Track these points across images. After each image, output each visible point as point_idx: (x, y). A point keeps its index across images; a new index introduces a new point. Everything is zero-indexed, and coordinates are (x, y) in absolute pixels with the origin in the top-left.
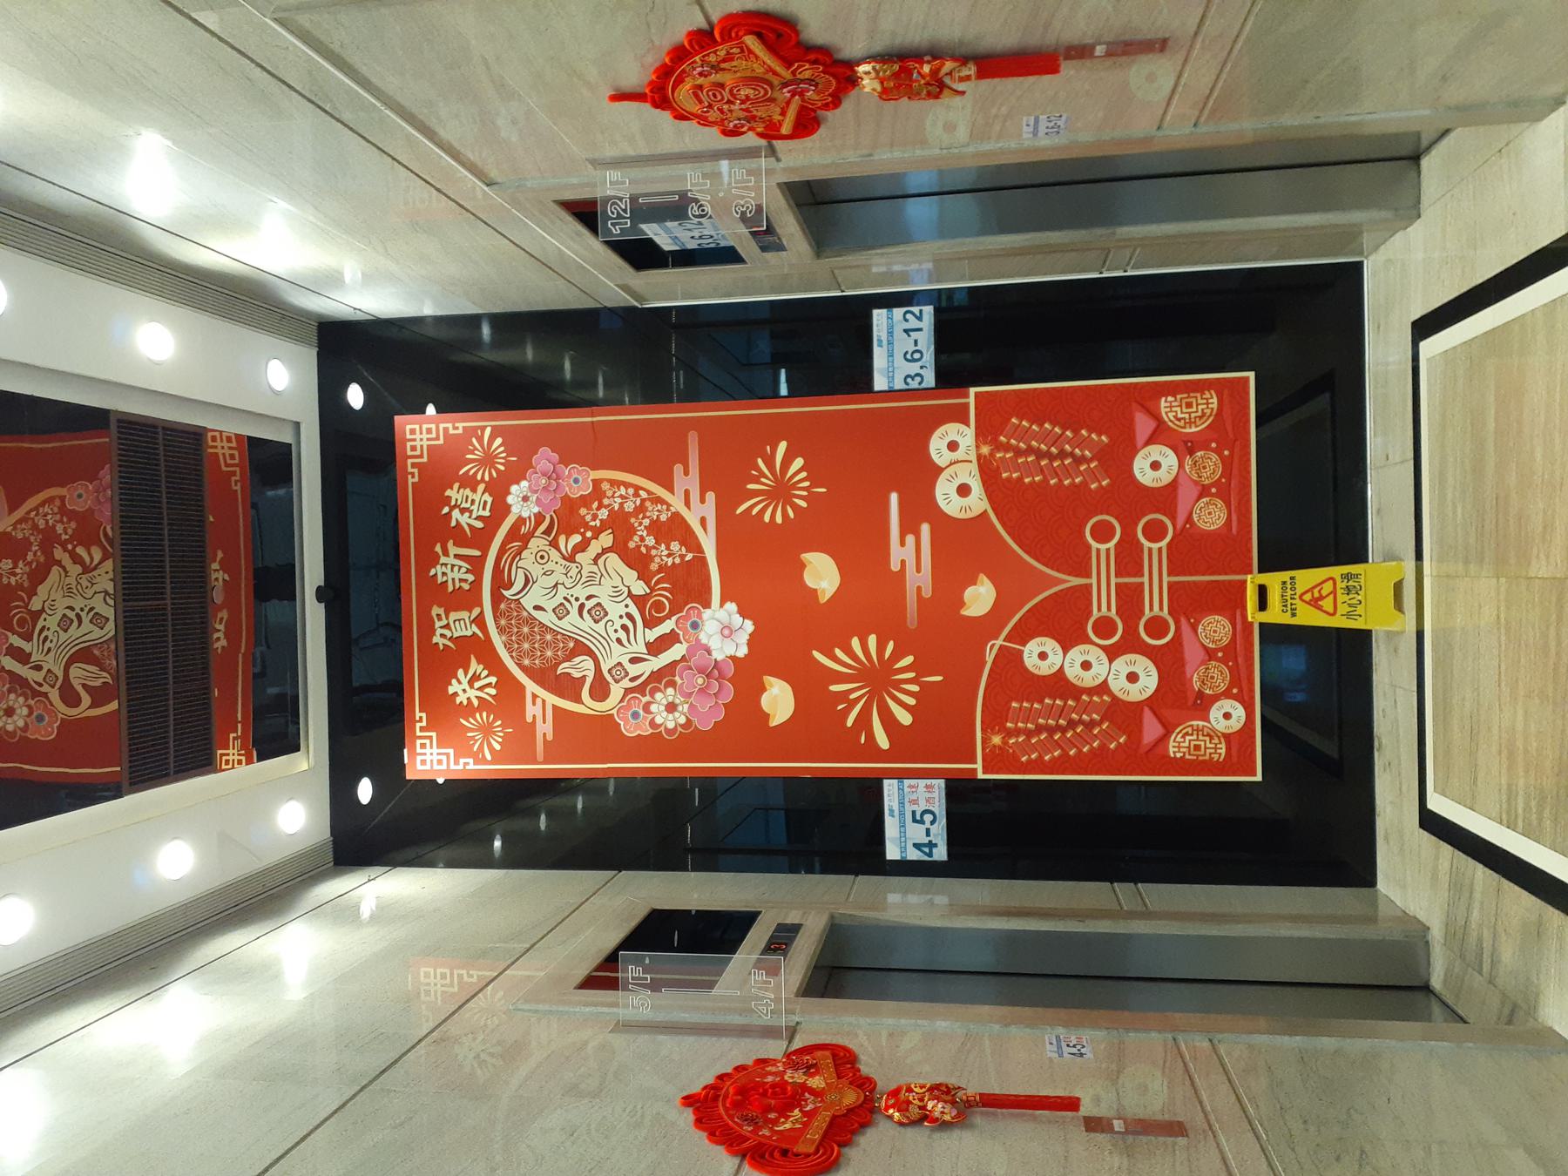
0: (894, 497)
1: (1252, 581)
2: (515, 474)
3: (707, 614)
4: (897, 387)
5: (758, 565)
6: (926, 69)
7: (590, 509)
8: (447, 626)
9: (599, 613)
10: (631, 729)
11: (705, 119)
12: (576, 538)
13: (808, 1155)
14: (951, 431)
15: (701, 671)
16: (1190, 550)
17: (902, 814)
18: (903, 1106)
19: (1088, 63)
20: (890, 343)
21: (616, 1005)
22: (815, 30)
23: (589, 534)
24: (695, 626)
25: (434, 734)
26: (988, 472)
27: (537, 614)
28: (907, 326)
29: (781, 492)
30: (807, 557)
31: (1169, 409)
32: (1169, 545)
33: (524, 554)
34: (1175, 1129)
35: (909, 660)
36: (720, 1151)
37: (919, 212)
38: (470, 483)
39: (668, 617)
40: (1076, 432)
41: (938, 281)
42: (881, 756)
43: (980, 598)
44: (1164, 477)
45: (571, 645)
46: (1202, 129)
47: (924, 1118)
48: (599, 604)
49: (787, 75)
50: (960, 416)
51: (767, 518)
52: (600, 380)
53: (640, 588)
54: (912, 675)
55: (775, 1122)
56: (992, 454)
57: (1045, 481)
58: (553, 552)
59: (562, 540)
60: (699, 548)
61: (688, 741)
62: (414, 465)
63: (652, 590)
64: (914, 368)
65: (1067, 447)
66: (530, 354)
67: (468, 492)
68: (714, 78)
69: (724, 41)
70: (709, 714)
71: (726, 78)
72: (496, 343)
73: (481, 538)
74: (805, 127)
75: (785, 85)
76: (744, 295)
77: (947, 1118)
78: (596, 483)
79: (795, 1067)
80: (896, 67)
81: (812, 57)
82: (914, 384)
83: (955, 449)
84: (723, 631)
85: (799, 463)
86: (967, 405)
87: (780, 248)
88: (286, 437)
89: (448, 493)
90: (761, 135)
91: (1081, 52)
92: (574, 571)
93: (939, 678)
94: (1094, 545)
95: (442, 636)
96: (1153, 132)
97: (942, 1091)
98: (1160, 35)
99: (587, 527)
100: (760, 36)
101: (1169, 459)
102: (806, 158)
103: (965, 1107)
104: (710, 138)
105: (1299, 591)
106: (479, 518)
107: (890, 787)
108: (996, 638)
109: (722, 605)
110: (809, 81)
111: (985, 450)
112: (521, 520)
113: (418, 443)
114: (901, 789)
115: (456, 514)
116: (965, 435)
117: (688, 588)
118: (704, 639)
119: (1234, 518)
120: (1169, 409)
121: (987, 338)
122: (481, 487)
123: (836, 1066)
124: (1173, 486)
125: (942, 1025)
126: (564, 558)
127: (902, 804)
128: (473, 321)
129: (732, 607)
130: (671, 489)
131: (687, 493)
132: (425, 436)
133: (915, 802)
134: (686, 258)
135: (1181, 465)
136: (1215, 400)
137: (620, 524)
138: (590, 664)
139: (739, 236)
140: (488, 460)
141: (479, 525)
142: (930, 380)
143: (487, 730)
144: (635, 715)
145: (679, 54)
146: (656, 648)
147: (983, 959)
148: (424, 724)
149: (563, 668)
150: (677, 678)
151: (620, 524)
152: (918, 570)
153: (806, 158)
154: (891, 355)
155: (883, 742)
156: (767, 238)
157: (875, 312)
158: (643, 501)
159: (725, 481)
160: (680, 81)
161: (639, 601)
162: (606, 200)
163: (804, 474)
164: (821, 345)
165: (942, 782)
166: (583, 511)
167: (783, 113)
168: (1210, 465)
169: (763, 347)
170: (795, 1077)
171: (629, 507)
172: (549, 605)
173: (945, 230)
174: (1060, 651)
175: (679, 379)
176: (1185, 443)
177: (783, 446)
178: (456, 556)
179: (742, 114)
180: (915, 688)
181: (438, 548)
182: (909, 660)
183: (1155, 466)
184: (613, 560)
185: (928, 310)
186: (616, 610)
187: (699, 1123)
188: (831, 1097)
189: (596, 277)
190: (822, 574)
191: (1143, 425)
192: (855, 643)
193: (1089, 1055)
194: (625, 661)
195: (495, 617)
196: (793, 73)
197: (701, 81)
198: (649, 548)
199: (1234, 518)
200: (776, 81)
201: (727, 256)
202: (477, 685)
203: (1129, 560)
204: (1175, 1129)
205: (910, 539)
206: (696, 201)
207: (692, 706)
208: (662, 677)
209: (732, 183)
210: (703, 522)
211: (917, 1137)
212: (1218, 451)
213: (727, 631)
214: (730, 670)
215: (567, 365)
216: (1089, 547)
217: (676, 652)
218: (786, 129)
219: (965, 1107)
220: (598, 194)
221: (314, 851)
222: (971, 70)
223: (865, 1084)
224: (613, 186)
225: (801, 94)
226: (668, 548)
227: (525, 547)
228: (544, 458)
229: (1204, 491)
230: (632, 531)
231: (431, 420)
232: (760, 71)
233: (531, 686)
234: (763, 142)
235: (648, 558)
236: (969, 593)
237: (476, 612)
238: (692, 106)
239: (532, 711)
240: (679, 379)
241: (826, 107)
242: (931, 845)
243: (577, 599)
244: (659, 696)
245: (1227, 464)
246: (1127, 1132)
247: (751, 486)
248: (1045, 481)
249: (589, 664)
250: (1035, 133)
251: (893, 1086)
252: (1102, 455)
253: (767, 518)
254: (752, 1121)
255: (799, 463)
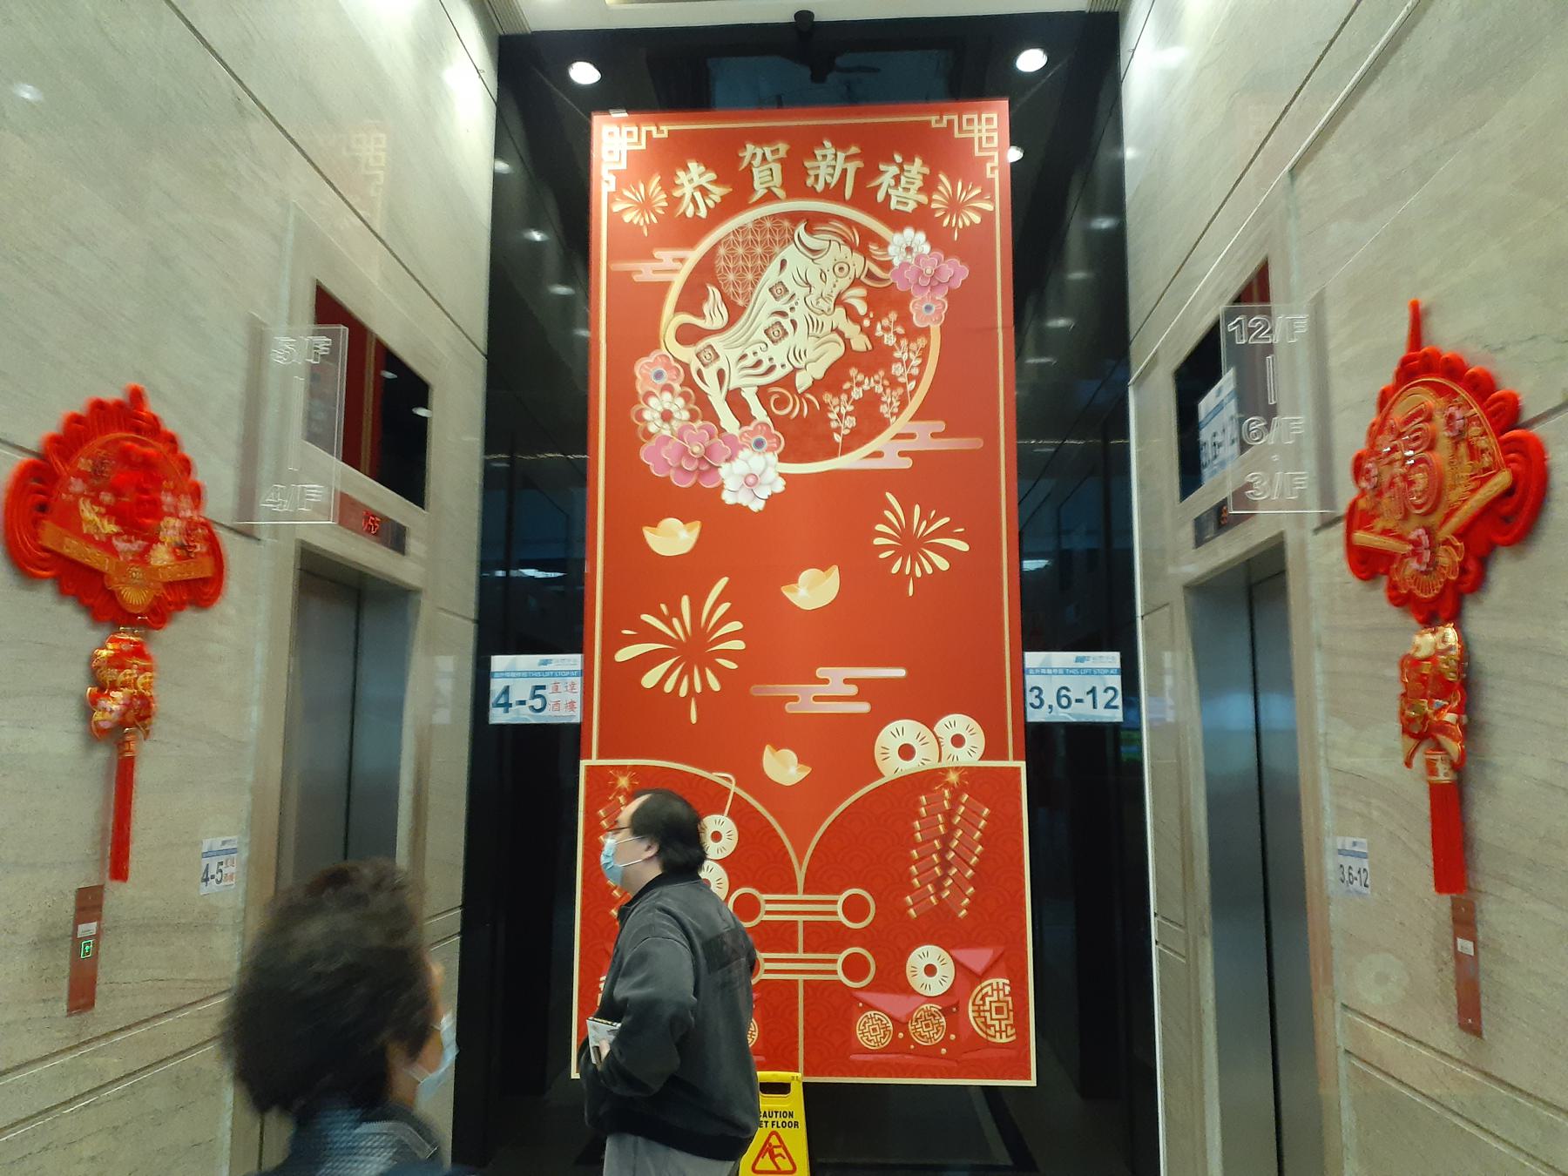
0: (901, 673)
1: (796, 1078)
2: (938, 238)
3: (772, 458)
4: (1028, 677)
5: (830, 517)
6: (1450, 717)
7: (896, 323)
8: (764, 159)
9: (775, 334)
10: (644, 370)
11: (1380, 432)
12: (862, 308)
13: (35, 537)
14: (976, 739)
15: (708, 451)
16: (832, 1007)
17: (543, 674)
18: (118, 661)
19: (1448, 929)
20: (1080, 671)
21: (291, 321)
22: (1506, 572)
23: (866, 323)
24: (759, 444)
25: (643, 146)
26: (929, 780)
27: (776, 263)
28: (1099, 692)
29: (910, 545)
30: (835, 572)
31: (996, 988)
32: (840, 983)
33: (846, 249)
34: (82, 995)
35: (715, 685)
36: (52, 425)
37: (1237, 710)
38: (929, 186)
39: (770, 414)
40: (972, 881)
41: (1151, 729)
42: (611, 646)
43: (783, 767)
44: (918, 980)
45: (740, 302)
46: (1343, 1061)
47: (102, 688)
48: (786, 333)
49: (1445, 532)
50: (994, 749)
51: (880, 527)
52: (1043, 360)
53: (803, 382)
54: (698, 688)
55: (96, 501)
56: (947, 785)
57: (916, 845)
58: (846, 282)
59: (862, 292)
60: (847, 448)
61: (628, 435)
62: (950, 122)
63: (801, 396)
64: (1050, 698)
65: (954, 871)
66: (1077, 275)
67: (919, 183)
68: (1444, 436)
69: (1502, 443)
70: (658, 459)
71: (1442, 454)
72: (1091, 236)
73: (865, 198)
74: (1363, 562)
75: (1429, 531)
76: (1142, 508)
77: (98, 716)
78: (926, 332)
79: (191, 527)
80: (1452, 677)
81: (1472, 566)
82: (1031, 698)
83: (954, 743)
84: (753, 476)
85: (943, 564)
86: (1005, 758)
87: (1199, 541)
89: (918, 161)
90: (1354, 505)
91: (1464, 923)
92: (823, 305)
93: (694, 719)
94: (841, 898)
95: (754, 155)
96: (1340, 999)
97: (140, 712)
98: (1486, 1027)
99: (873, 322)
100: (1508, 493)
101: (937, 986)
102: (1320, 563)
103: (120, 735)
104: (1351, 438)
105: (781, 1131)
106: (888, 197)
107: (574, 661)
108: (737, 784)
109: (781, 475)
110: (1433, 564)
111: (953, 778)
112: (883, 244)
113: (976, 126)
114: (570, 674)
115: (894, 170)
116: (971, 754)
117: (804, 437)
118: (744, 454)
119: (870, 1057)
120: (996, 988)
121: (1083, 781)
122: (924, 199)
123: (187, 581)
124: (908, 990)
125: (255, 713)
126: (839, 295)
127: (554, 674)
128: (1116, 204)
129: (780, 486)
130: (917, 417)
131: (911, 436)
132: (984, 135)
133: (556, 690)
134: (1188, 422)
135: (930, 999)
136: (1005, 1040)
137: (877, 359)
138: (719, 322)
139: (1222, 483)
140: (954, 207)
141: (880, 197)
142: (1035, 716)
143: (646, 205)
144: (659, 375)
145: (1482, 386)
146: (735, 401)
147: (368, 760)
148: (655, 135)
149: (714, 293)
150: (700, 423)
151: (877, 359)
152: (816, 699)
153: (1320, 563)
154: (1066, 672)
155: (623, 655)
156: (1220, 520)
157: (1117, 655)
158: (904, 385)
159: (924, 480)
160: (1440, 390)
161: (788, 381)
162: (1267, 312)
163: (929, 570)
164: (1082, 597)
165: (577, 719)
166: (893, 316)
167: (1385, 532)
168: (929, 1032)
169: (1078, 542)
170: (171, 529)
171: (897, 369)
172: (786, 278)
173: (1214, 740)
174: (720, 856)
175: (1046, 446)
176: (956, 1005)
177: (963, 546)
178: (844, 171)
179: (1386, 479)
180: (683, 692)
181: (854, 150)
182: (715, 685)
183: (930, 970)
184: (836, 351)
185: (1117, 716)
186: (778, 353)
187: (99, 406)
188: (136, 573)
189: (1170, 312)
190: (814, 590)
191: (978, 958)
192: (736, 626)
193: (204, 889)
194: (721, 364)
195: (774, 217)
196: (1447, 542)
197: (1440, 420)
198: (848, 392)
199: (870, 1057)
200: (1435, 519)
201: (1191, 471)
202: (698, 195)
203: (824, 937)
204: (82, 995)
205: (852, 690)
206: (1268, 427)
207: (668, 439)
208: (702, 407)
209: (1288, 473)
210: (877, 455)
211: (77, 680)
212: (945, 1042)
213: (751, 481)
214: (708, 485)
215: (1061, 322)
216: (839, 892)
217: (729, 422)
218: (1361, 537)
219: (120, 735)
220: (1276, 304)
221: (515, 13)
222: (1444, 775)
223: (158, 615)
224: (1287, 324)
225: (1416, 554)
226: (848, 414)
227: (853, 247)
228: (955, 271)
229: (900, 1024)
230: (869, 372)
231: (1002, 157)
232: (1453, 497)
233: (694, 256)
234: (1342, 509)
235: (837, 390)
236: (789, 755)
237: (780, 193)
238: (1398, 414)
239: (666, 256)
240: (1046, 446)
241: (1393, 587)
242: (507, 705)
243: (792, 309)
244: (680, 402)
245: (930, 1052)
246: (76, 941)
247: (917, 509)
248: (916, 845)
249: (719, 322)
250: (1340, 852)
251: (149, 650)
252: (944, 911)
253: (880, 527)
254: (96, 473)
255: (943, 564)
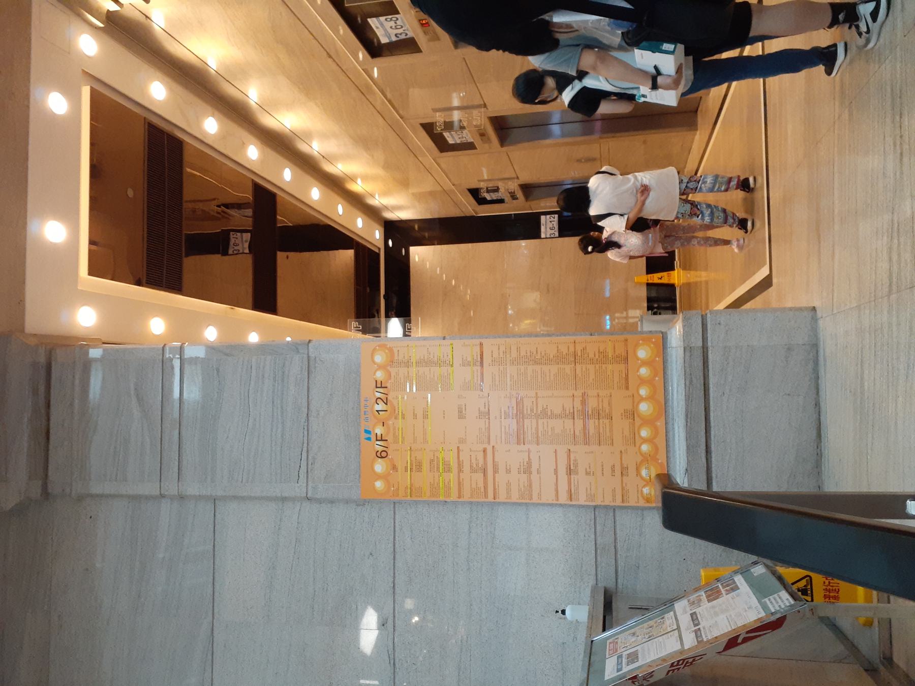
64: (553, 232)
87: (517, 199)
88: (377, 251)
189: (469, 208)
201: (501, 201)
